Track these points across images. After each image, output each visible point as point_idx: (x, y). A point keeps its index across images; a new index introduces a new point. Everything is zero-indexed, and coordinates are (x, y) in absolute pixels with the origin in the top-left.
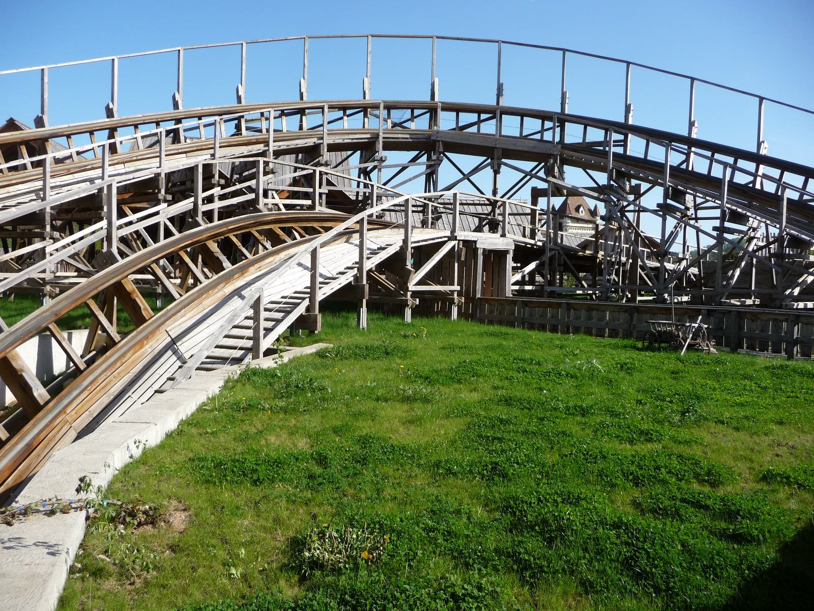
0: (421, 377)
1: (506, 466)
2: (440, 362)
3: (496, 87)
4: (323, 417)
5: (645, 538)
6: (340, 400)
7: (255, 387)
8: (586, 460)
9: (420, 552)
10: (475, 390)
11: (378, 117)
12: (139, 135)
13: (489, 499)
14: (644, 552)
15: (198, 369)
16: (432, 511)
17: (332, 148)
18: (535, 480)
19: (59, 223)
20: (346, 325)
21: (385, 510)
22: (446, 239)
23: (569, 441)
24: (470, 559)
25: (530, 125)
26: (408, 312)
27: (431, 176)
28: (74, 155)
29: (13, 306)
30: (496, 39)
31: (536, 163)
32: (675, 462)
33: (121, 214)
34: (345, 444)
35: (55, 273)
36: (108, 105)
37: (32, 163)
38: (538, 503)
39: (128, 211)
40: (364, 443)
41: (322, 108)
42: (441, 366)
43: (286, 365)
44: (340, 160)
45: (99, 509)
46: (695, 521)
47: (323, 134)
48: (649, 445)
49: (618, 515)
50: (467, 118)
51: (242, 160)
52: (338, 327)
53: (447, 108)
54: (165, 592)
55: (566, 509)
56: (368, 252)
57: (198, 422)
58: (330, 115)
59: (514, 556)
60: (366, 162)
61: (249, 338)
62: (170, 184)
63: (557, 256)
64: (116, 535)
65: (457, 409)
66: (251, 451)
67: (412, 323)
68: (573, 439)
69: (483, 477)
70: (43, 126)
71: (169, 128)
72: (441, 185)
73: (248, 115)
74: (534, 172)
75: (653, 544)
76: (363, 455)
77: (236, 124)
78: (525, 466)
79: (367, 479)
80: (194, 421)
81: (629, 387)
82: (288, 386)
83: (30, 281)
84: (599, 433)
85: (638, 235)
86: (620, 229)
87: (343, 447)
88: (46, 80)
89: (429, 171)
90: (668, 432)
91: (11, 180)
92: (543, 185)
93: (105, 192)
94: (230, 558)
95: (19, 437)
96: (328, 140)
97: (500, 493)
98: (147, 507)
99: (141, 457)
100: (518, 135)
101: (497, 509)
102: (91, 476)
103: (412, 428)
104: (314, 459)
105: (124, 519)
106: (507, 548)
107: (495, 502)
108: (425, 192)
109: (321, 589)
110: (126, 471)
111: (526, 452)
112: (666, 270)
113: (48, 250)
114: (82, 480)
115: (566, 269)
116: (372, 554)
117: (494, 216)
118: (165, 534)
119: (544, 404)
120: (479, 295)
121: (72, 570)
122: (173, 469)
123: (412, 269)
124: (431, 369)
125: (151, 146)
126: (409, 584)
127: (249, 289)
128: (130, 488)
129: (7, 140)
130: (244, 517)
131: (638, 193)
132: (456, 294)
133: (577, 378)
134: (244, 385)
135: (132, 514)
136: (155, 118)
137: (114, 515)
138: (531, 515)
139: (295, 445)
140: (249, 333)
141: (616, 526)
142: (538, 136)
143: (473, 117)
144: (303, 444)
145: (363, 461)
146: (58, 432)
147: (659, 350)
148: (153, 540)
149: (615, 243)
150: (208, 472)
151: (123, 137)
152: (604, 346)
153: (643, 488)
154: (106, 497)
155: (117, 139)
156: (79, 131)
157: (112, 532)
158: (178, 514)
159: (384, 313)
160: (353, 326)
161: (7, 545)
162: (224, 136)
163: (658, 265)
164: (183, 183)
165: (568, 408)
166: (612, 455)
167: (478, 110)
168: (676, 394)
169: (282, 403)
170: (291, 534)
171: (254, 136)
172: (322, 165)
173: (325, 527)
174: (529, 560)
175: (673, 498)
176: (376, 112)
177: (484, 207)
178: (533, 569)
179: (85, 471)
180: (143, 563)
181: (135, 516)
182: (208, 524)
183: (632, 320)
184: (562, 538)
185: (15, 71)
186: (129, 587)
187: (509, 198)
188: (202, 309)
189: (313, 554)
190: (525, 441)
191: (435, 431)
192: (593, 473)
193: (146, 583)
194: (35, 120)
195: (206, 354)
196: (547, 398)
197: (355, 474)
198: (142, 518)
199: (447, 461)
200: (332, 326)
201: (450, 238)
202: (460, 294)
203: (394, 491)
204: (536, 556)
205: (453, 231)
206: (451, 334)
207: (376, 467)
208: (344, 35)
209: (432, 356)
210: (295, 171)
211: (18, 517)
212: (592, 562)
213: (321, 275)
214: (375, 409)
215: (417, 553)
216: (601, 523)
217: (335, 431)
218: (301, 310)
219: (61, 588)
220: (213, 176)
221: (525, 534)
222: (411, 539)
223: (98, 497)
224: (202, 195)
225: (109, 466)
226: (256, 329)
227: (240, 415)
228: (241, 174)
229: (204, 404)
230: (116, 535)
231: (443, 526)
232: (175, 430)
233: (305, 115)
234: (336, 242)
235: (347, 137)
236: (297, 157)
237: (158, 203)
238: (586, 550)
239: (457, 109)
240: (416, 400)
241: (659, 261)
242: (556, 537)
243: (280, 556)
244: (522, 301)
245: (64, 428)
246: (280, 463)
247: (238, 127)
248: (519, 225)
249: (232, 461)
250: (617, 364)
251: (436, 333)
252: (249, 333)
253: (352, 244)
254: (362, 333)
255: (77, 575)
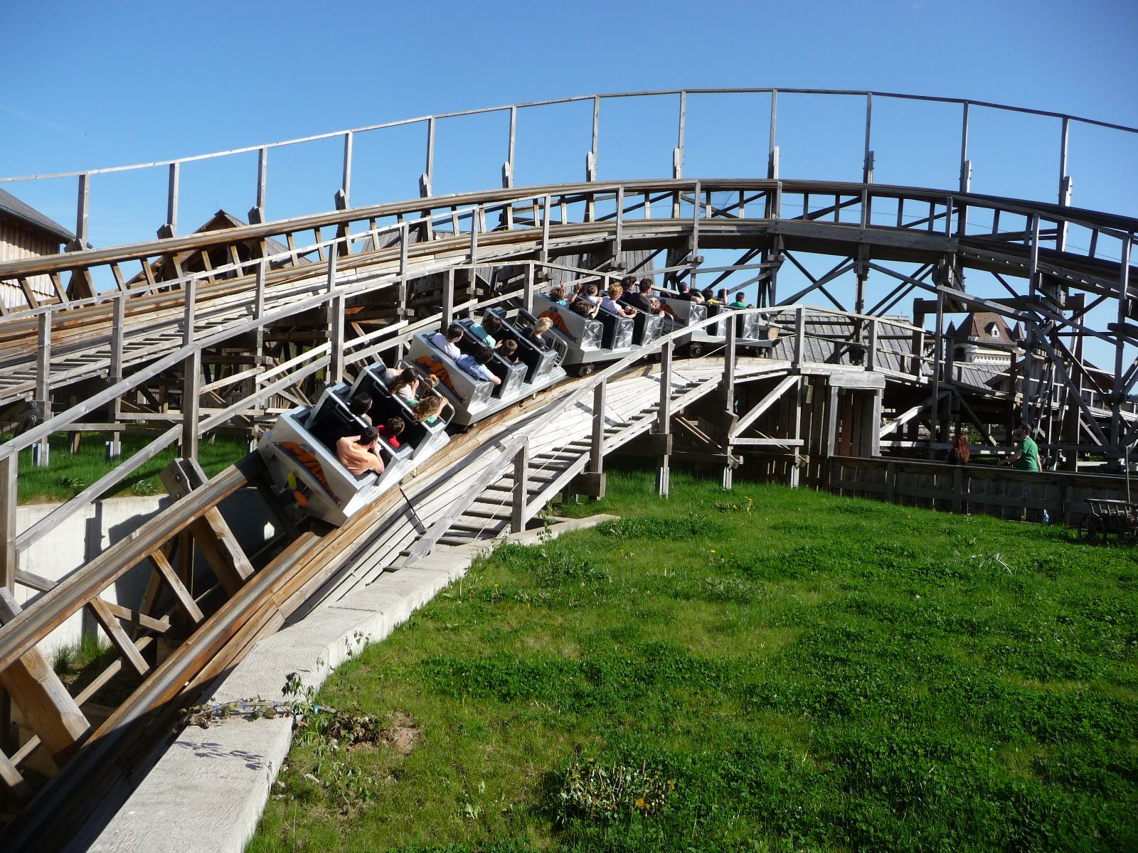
0: (739, 567)
1: (848, 699)
2: (768, 548)
3: (863, 157)
4: (599, 616)
5: (1044, 816)
6: (624, 594)
7: (512, 571)
8: (969, 699)
9: (715, 807)
10: (815, 589)
11: (693, 202)
12: (375, 232)
13: (820, 743)
14: (1038, 836)
15: (440, 542)
16: (737, 753)
17: (629, 245)
18: (889, 722)
19: (273, 344)
20: (641, 491)
21: (673, 746)
22: (785, 373)
23: (946, 670)
24: (783, 821)
25: (916, 211)
26: (728, 475)
27: (766, 283)
28: (295, 259)
29: (214, 450)
30: (864, 90)
31: (921, 265)
32: (1107, 713)
33: (350, 334)
34: (626, 654)
35: (266, 409)
36: (338, 194)
37: (244, 269)
38: (890, 754)
39: (359, 330)
40: (652, 654)
41: (616, 191)
42: (768, 552)
43: (554, 542)
44: (640, 261)
45: (309, 716)
46: (1127, 799)
47: (616, 227)
48: (1070, 685)
49: (1007, 780)
50: (819, 202)
51: (506, 263)
52: (629, 492)
53: (791, 187)
54: (384, 827)
55: (929, 765)
56: (674, 389)
57: (435, 614)
58: (626, 201)
59: (847, 824)
60: (675, 265)
61: (507, 504)
62: (413, 295)
63: (950, 399)
64: (328, 750)
65: (786, 615)
66: (501, 655)
67: (732, 490)
68: (952, 667)
69: (814, 711)
70: (259, 221)
71: (413, 222)
72: (780, 296)
73: (516, 203)
74: (917, 278)
75: (1055, 826)
76: (649, 671)
77: (501, 215)
78: (876, 701)
79: (653, 703)
80: (431, 612)
81: (1047, 597)
82: (555, 571)
83: (237, 419)
84: (993, 661)
85: (1078, 370)
86: (1049, 360)
87: (623, 658)
88: (264, 163)
89: (764, 276)
90: (1104, 666)
91: (218, 290)
92: (930, 296)
93: (331, 305)
94: (466, 793)
95: (215, 619)
96: (622, 235)
97: (836, 737)
98: (367, 719)
99: (362, 655)
100: (895, 225)
101: (830, 758)
102: (301, 674)
103: (721, 637)
104: (584, 672)
105: (339, 732)
106: (838, 812)
107: (828, 748)
108: (758, 307)
109: (580, 843)
110: (343, 671)
111: (880, 682)
112: (1124, 423)
113: (258, 380)
114: (290, 677)
115: (963, 418)
116: (650, 803)
117: (857, 340)
118: (388, 755)
119: (913, 614)
120: (831, 453)
121: (274, 790)
122: (401, 672)
123: (734, 415)
124: (754, 557)
125: (390, 245)
126: (696, 847)
127: (510, 437)
128: (347, 694)
129: (216, 239)
130: (486, 740)
131: (1078, 307)
132: (797, 451)
133: (969, 579)
134: (497, 567)
135: (349, 727)
136: (396, 208)
137: (326, 724)
138: (877, 770)
139: (560, 652)
140: (508, 496)
141: (1003, 795)
142: (925, 226)
143: (828, 201)
144: (570, 651)
145: (650, 679)
146: (262, 616)
147: (1104, 543)
148: (372, 762)
149: (1042, 380)
150: (444, 680)
151: (356, 234)
152: (1018, 534)
153: (1053, 746)
154: (317, 702)
155: (349, 237)
156: (302, 227)
157: (323, 745)
158: (404, 731)
159: (694, 475)
160: (650, 491)
161: (201, 751)
162: (484, 231)
163: (1110, 414)
164: (430, 294)
165: (949, 623)
166: (1008, 694)
167: (836, 190)
168: (1121, 610)
169: (546, 595)
170: (547, 768)
171: (523, 230)
172: (614, 269)
173: (590, 763)
174: (868, 832)
175: (1096, 764)
176: (691, 196)
177: (845, 327)
178: (872, 843)
179: (293, 667)
180: (358, 789)
181: (352, 729)
182: (441, 746)
183: (1063, 496)
184: (919, 805)
185: (228, 153)
186: (341, 818)
187: (879, 316)
188: (448, 462)
189: (572, 796)
190: (879, 666)
191: (752, 643)
192: (977, 718)
193: (362, 814)
194: (249, 214)
195: (450, 522)
196: (919, 606)
197: (637, 696)
198: (360, 732)
199: (764, 687)
200: (620, 491)
201: (794, 371)
202: (803, 450)
203: (687, 722)
204: (879, 827)
205: (795, 362)
206: (786, 507)
207: (666, 687)
208: (649, 91)
209: (756, 538)
210: (578, 277)
211: (214, 719)
212: (959, 843)
213: (607, 421)
214: (670, 608)
215: (711, 808)
216: (979, 788)
217: (615, 635)
218: (578, 468)
219: (261, 810)
220: (468, 285)
221: (866, 796)
222: (704, 788)
223: (308, 701)
224: (453, 310)
225: (323, 664)
226: (517, 493)
227: (489, 608)
228: (505, 281)
229: (445, 590)
230: (328, 750)
231: (751, 775)
232: (406, 622)
233: (593, 201)
234: (630, 375)
235: (649, 230)
236: (581, 258)
237: (396, 320)
238: (952, 825)
239: (806, 189)
240: (729, 599)
241: (1111, 408)
242: (910, 804)
243: (531, 796)
244: (896, 464)
245: (269, 612)
246: (538, 674)
247: (503, 218)
248: (895, 354)
249: (477, 667)
250: (1033, 561)
251: (766, 506)
252: (508, 496)
253: (652, 378)
254: (662, 502)
255: (280, 796)
